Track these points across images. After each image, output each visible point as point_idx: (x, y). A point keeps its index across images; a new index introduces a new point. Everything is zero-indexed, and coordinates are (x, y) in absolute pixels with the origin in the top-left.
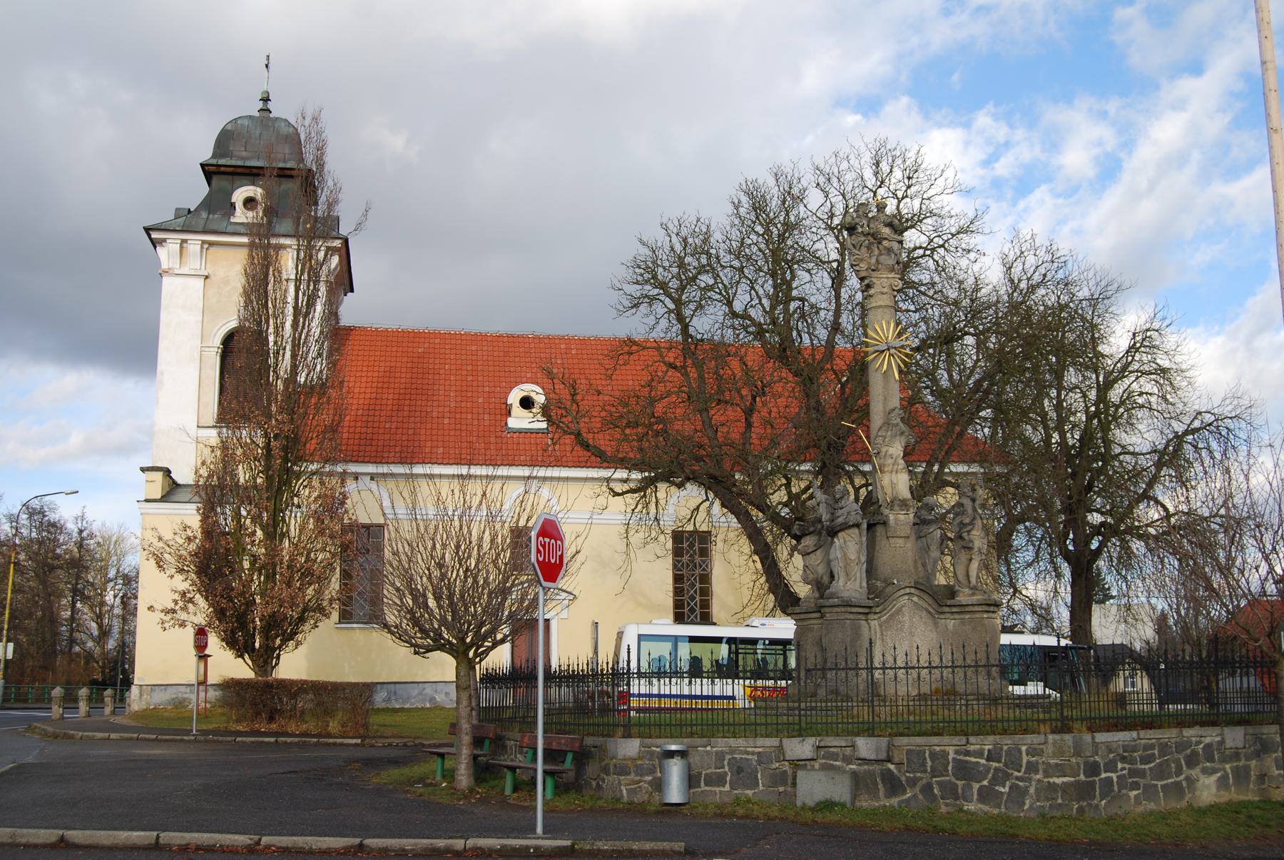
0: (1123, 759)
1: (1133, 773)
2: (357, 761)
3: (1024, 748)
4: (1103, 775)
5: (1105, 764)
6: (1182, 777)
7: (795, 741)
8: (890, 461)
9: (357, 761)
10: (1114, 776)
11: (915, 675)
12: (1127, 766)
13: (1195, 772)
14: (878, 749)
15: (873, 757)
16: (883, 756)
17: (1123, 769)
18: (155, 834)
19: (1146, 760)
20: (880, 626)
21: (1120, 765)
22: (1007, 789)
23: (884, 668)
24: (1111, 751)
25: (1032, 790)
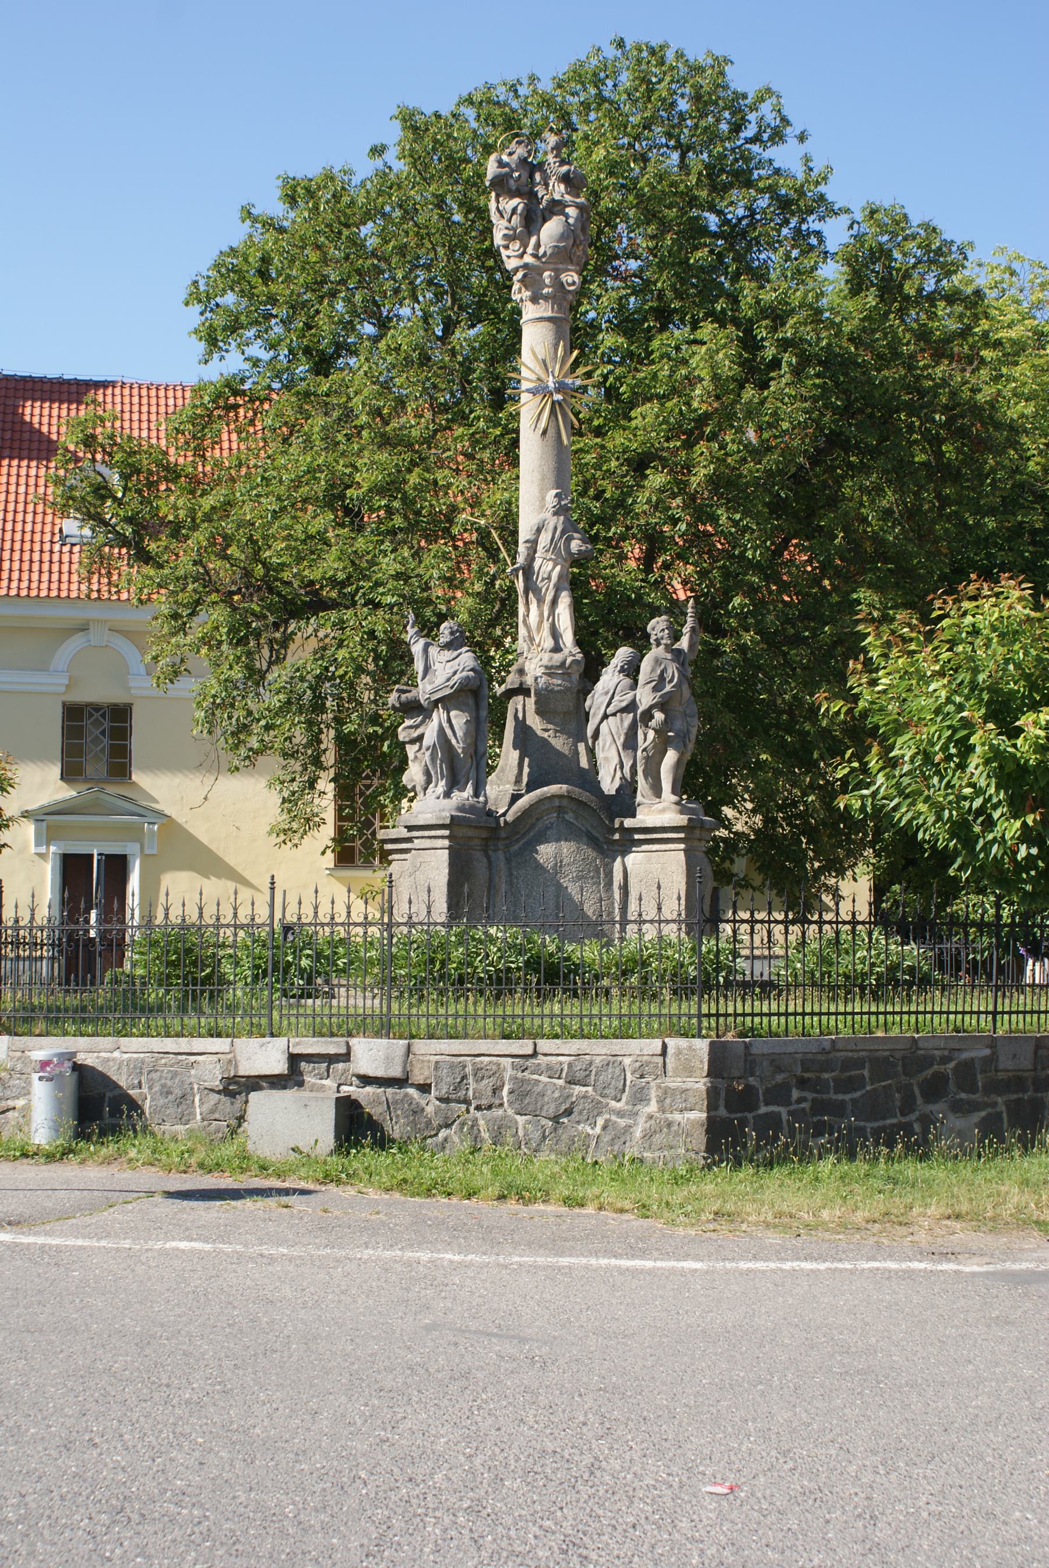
0: (802, 1083)
1: (819, 1107)
2: (746, 986)
3: (627, 1061)
4: (763, 1110)
5: (767, 1091)
6: (913, 1117)
7: (255, 1042)
9: (746, 986)
10: (783, 1111)
11: (831, 935)
12: (810, 1096)
13: (938, 1109)
14: (388, 1060)
15: (380, 1073)
16: (396, 1072)
17: (800, 1100)
18: (656, 1045)
19: (847, 1085)
20: (508, 860)
21: (795, 1094)
22: (598, 1129)
23: (641, 922)
24: (779, 1069)
25: (638, 1133)
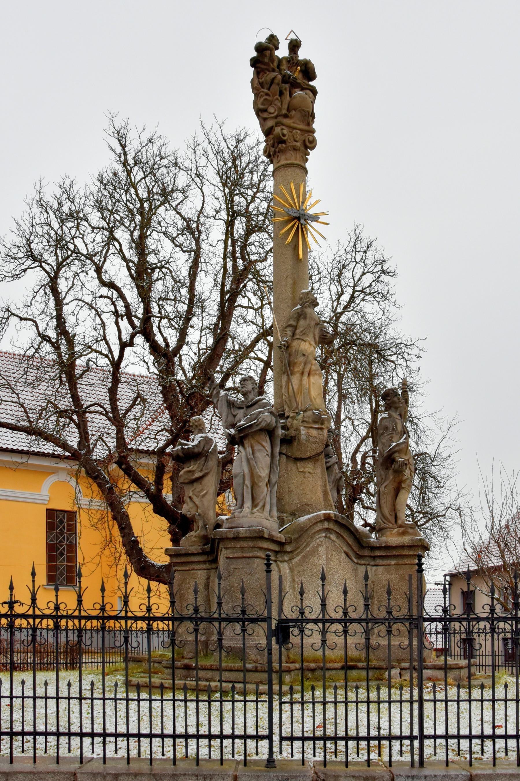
8: (301, 359)
20: (291, 570)
